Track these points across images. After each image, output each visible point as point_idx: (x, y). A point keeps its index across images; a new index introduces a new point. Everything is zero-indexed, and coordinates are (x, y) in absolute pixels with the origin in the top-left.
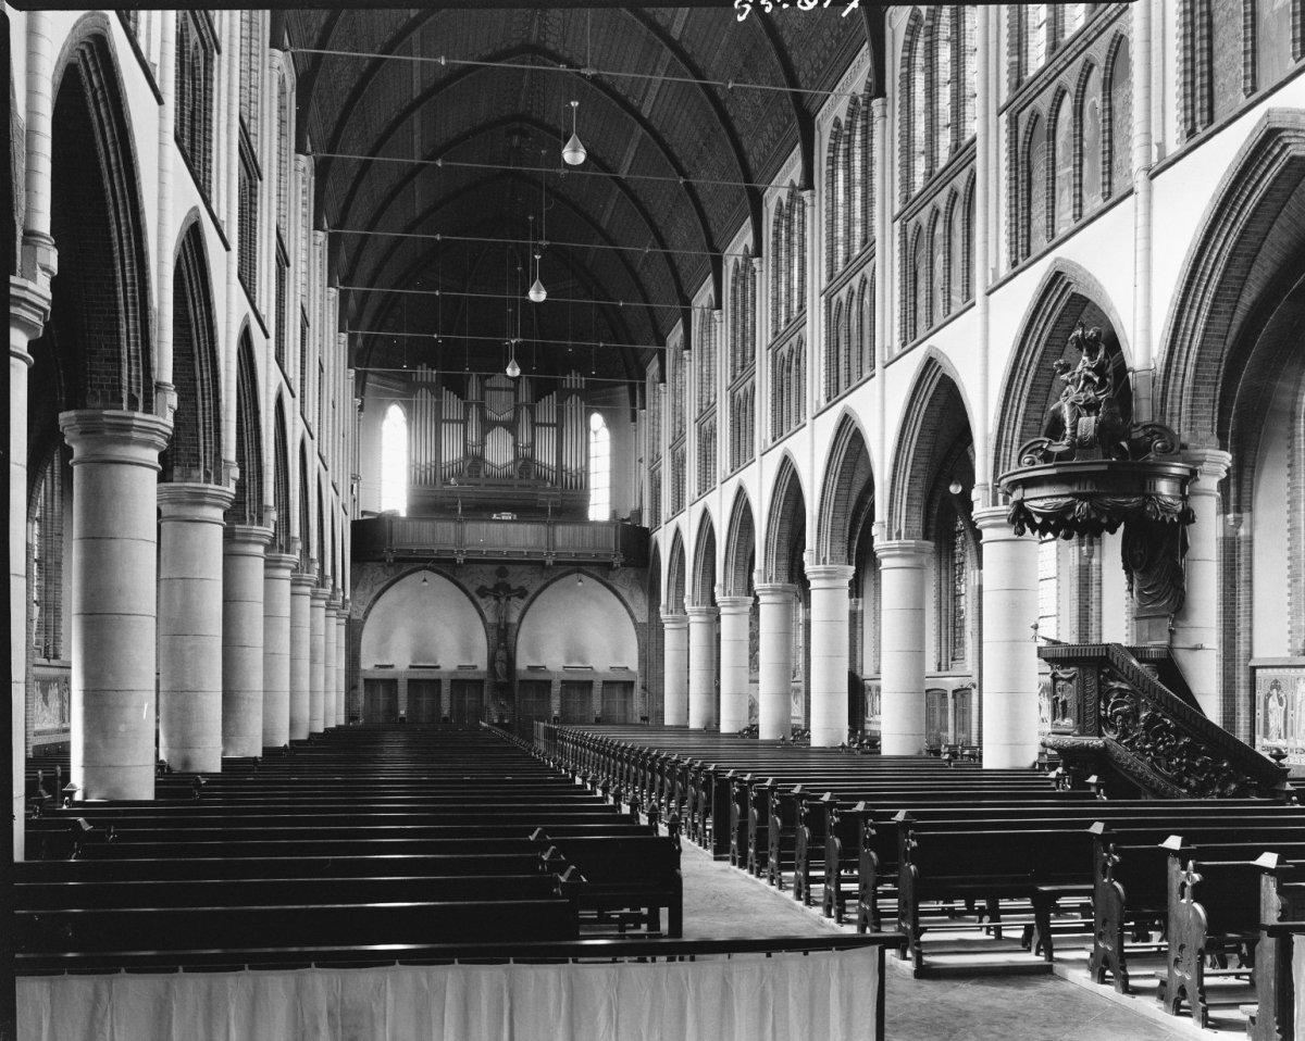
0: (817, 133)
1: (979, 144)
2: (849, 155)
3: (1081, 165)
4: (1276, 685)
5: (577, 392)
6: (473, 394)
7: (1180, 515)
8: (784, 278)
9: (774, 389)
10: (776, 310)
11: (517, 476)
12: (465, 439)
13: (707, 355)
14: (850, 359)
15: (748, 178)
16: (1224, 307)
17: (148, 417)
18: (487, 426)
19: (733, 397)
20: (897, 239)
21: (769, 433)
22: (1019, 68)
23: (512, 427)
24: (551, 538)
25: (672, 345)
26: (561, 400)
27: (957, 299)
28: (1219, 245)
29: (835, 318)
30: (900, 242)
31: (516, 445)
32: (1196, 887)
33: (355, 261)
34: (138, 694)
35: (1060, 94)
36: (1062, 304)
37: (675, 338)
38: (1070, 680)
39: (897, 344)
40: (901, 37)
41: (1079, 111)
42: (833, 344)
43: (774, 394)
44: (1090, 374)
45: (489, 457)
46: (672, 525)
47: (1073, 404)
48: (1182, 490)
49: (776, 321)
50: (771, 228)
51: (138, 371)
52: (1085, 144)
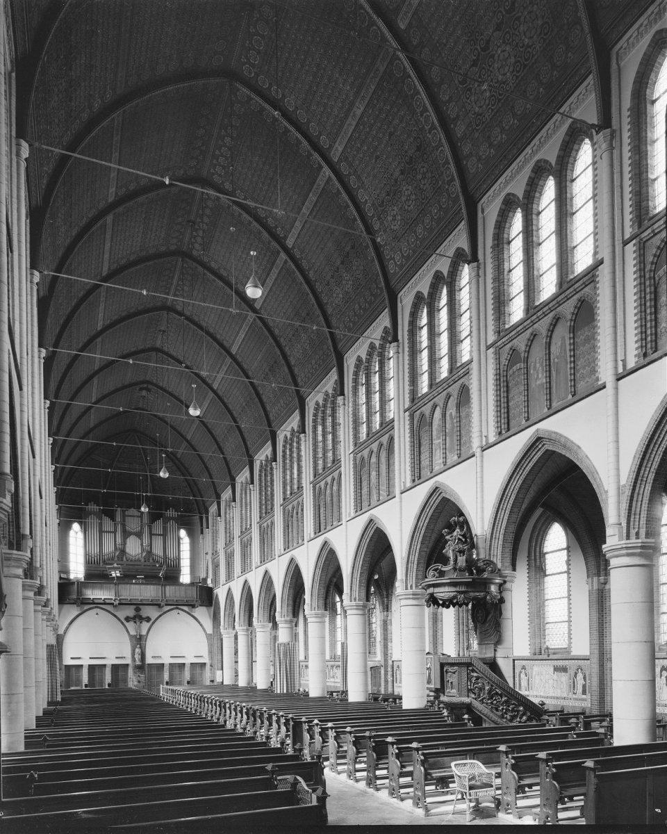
0: (307, 407)
1: (396, 423)
2: (324, 420)
3: (445, 440)
4: (524, 668)
5: (173, 519)
6: (118, 519)
7: (499, 600)
8: (288, 472)
9: (284, 525)
10: (284, 487)
11: (143, 560)
12: (115, 541)
13: (248, 505)
14: (327, 515)
15: (270, 425)
16: (516, 510)
17: (20, 553)
18: (126, 534)
19: (260, 527)
20: (352, 462)
21: (282, 547)
22: (413, 392)
23: (139, 535)
24: (164, 593)
25: (224, 499)
26: (165, 523)
27: (383, 493)
28: (514, 484)
29: (318, 495)
30: (353, 464)
31: (142, 545)
32: (512, 765)
33: (60, 452)
34: (16, 696)
35: (435, 406)
36: (438, 501)
37: (226, 495)
38: (454, 673)
39: (353, 511)
40: (352, 369)
41: (444, 415)
42: (317, 508)
43: (284, 528)
44: (461, 537)
45: (128, 550)
46: (226, 587)
47: (453, 550)
48: (500, 589)
49: (284, 493)
50: (281, 449)
51: (13, 529)
52: (447, 431)
